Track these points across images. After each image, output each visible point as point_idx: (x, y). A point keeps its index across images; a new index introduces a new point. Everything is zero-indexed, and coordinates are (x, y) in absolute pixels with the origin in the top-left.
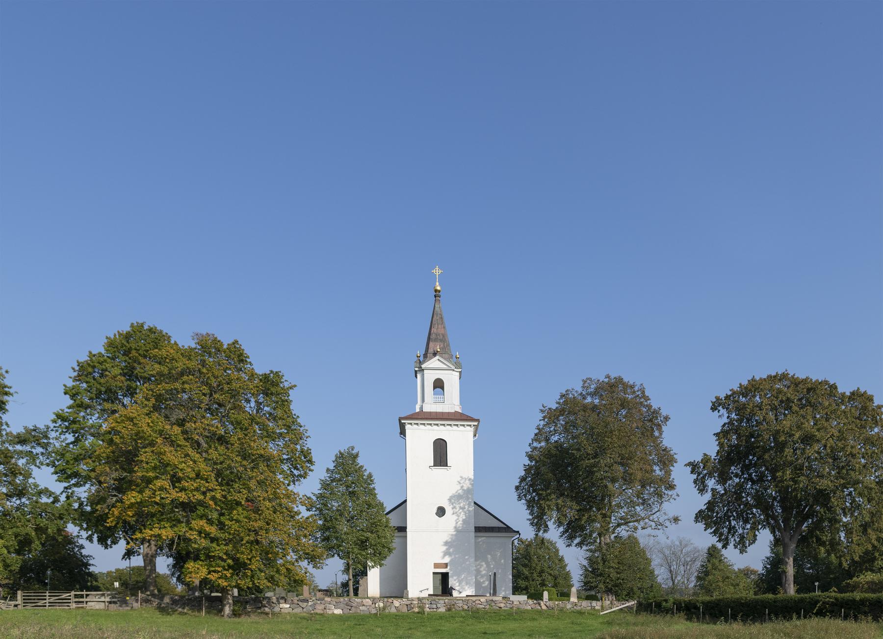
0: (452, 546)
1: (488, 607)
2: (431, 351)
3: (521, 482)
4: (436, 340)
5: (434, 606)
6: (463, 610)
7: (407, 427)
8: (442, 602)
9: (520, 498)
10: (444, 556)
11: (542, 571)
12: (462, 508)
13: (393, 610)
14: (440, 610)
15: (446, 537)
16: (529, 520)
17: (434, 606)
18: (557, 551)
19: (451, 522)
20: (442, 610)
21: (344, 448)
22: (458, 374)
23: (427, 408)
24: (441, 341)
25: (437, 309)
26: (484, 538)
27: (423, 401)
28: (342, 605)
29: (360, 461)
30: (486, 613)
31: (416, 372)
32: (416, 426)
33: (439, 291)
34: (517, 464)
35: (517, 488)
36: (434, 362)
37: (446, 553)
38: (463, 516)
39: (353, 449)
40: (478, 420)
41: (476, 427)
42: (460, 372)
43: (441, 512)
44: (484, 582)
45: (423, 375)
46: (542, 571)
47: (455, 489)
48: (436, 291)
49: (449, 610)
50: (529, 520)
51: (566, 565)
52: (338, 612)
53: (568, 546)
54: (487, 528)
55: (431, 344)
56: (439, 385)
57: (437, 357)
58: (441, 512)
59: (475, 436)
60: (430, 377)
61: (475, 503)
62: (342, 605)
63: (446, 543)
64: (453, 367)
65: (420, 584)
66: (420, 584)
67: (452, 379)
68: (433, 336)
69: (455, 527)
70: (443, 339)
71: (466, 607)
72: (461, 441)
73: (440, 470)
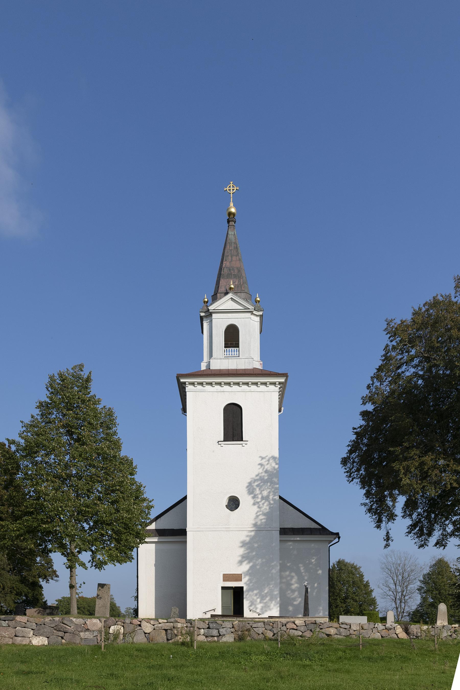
0: (253, 548)
1: (308, 634)
2: (222, 289)
3: (351, 452)
4: (229, 276)
5: (215, 632)
6: (266, 639)
7: (189, 388)
8: (229, 625)
9: (350, 474)
10: (241, 562)
11: (346, 598)
12: (265, 498)
13: (140, 639)
14: (224, 639)
15: (244, 536)
16: (365, 504)
17: (215, 632)
18: (362, 576)
19: (249, 514)
20: (229, 638)
21: (65, 365)
22: (258, 319)
23: (216, 365)
24: (235, 276)
25: (230, 236)
26: (295, 544)
27: (211, 355)
28: (47, 629)
29: (95, 389)
30: (309, 644)
31: (202, 318)
32: (200, 387)
33: (234, 214)
34: (346, 420)
35: (344, 461)
36: (225, 303)
37: (245, 558)
38: (265, 507)
39: (81, 367)
40: (285, 375)
41: (283, 386)
42: (261, 316)
43: (233, 503)
44: (294, 599)
45: (211, 321)
46: (346, 598)
47: (253, 471)
48: (230, 214)
49: (241, 639)
50: (365, 504)
51: (372, 591)
52: (39, 641)
53: (421, 546)
54: (296, 531)
55: (222, 282)
56: (232, 337)
57: (230, 295)
58: (233, 503)
59: (280, 411)
60: (220, 324)
61: (280, 498)
62: (47, 629)
63: (244, 544)
64: (251, 308)
65: (203, 601)
66: (203, 601)
67: (250, 327)
68: (225, 271)
69: (255, 525)
70: (237, 275)
71: (270, 634)
72: (261, 405)
73: (233, 447)
